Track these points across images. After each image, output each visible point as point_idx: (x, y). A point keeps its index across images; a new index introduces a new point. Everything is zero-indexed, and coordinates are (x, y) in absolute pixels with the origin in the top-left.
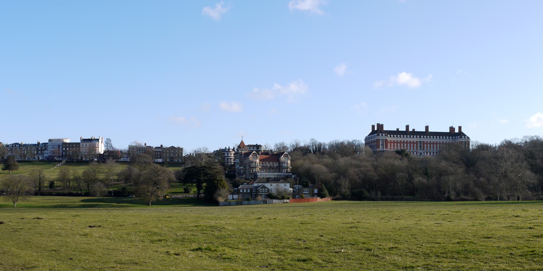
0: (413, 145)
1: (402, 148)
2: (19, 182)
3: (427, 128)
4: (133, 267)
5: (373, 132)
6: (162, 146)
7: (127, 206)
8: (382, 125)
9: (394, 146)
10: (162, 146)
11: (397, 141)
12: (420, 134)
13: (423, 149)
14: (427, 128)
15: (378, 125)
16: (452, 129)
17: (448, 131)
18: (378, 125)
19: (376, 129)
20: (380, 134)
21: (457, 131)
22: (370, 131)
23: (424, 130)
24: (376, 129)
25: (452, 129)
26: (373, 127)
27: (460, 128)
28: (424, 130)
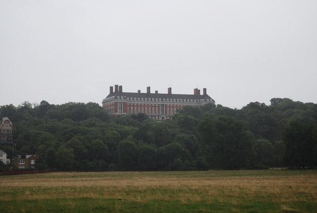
1: (139, 112)
3: (170, 89)
5: (111, 93)
6: (139, 91)
7: (61, 177)
8: (121, 87)
10: (139, 91)
12: (163, 96)
13: (166, 113)
14: (170, 89)
15: (116, 86)
17: (192, 93)
18: (116, 86)
19: (114, 91)
21: (202, 93)
22: (108, 93)
23: (146, 92)
24: (114, 91)
26: (111, 88)
27: (205, 90)
28: (146, 92)
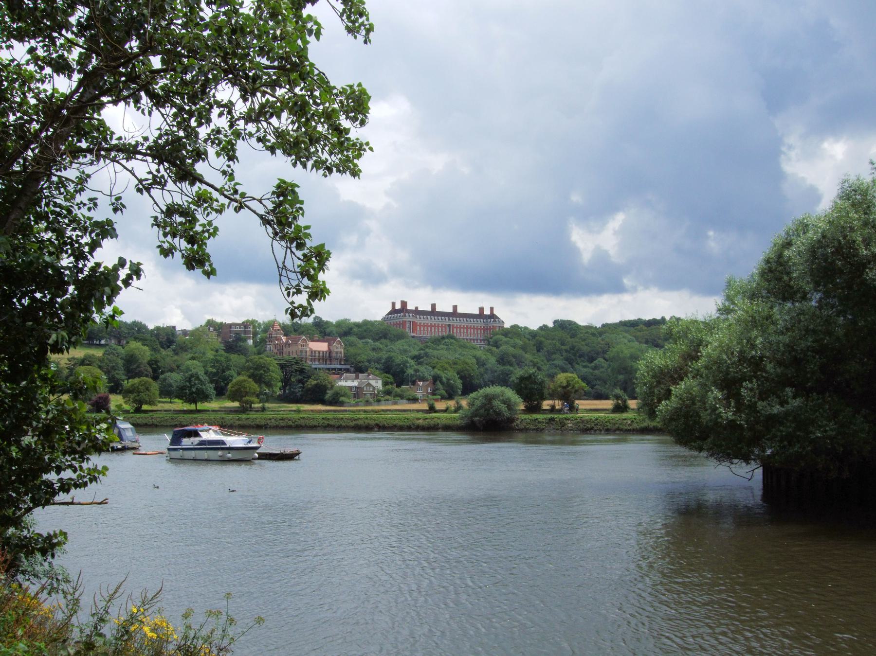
5: (394, 311)
16: (481, 310)
25: (481, 310)
27: (492, 309)
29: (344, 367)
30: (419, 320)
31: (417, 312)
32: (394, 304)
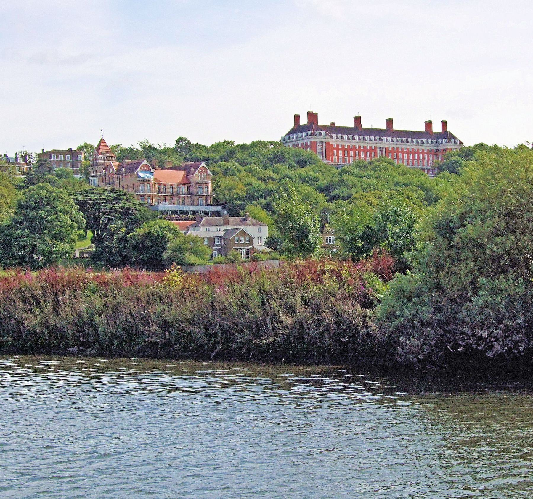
0: (349, 154)
2: (343, 240)
4: (209, 494)
5: (298, 128)
9: (343, 156)
11: (349, 146)
20: (317, 132)
22: (291, 125)
25: (428, 125)
27: (444, 124)
29: (212, 208)
30: (336, 141)
31: (332, 129)
32: (297, 118)
